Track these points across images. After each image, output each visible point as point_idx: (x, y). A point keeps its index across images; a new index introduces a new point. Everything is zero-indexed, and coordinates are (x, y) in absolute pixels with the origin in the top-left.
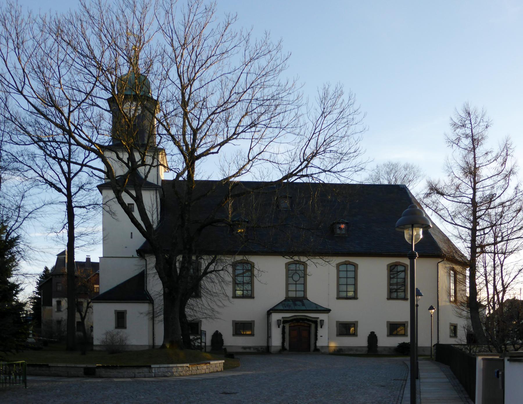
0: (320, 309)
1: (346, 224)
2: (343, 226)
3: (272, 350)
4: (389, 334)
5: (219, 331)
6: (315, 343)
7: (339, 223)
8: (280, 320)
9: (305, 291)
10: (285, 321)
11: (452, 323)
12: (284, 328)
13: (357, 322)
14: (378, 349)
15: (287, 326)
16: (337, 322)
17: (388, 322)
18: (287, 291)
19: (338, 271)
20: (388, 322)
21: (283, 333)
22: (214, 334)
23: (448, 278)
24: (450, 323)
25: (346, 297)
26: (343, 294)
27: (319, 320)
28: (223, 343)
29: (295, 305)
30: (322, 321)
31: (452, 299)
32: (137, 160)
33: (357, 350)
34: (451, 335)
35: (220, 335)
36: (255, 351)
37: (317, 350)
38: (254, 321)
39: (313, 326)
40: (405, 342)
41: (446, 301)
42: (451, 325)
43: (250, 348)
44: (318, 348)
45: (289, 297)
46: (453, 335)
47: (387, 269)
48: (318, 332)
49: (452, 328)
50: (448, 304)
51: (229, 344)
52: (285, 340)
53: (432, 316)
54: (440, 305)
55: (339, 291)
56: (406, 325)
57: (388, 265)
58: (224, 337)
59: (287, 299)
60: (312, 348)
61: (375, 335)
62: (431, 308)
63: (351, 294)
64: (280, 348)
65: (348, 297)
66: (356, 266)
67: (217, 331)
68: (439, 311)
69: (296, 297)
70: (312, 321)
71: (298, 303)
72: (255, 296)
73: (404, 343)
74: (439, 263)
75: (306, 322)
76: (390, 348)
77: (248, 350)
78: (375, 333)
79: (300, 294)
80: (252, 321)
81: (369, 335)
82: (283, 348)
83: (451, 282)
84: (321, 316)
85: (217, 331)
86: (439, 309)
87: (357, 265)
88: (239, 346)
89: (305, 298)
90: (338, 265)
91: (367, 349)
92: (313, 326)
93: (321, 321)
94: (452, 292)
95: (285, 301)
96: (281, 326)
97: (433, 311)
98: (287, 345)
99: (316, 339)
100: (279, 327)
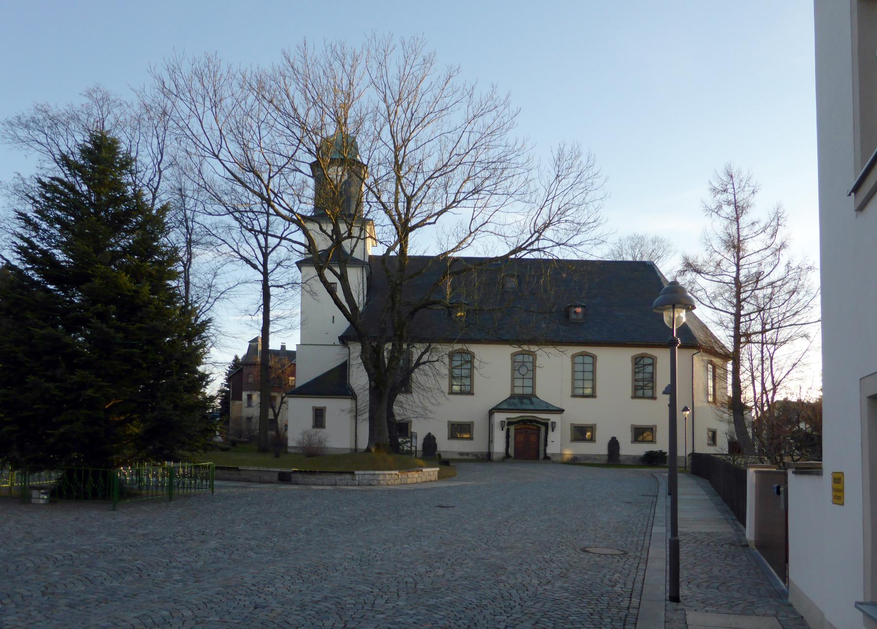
1: (582, 307)
2: (579, 310)
3: (494, 457)
6: (545, 450)
8: (505, 422)
9: (533, 387)
10: (510, 423)
14: (620, 458)
17: (632, 426)
18: (513, 387)
20: (632, 426)
21: (508, 437)
26: (580, 392)
27: (550, 423)
30: (554, 424)
31: (711, 399)
33: (595, 459)
35: (434, 438)
36: (474, 458)
37: (547, 458)
40: (654, 450)
42: (709, 430)
43: (467, 454)
44: (548, 455)
46: (712, 443)
47: (632, 362)
50: (706, 404)
55: (574, 388)
56: (654, 429)
57: (632, 357)
60: (542, 455)
61: (617, 441)
63: (588, 391)
66: (594, 357)
67: (430, 434)
71: (526, 401)
74: (694, 354)
76: (634, 457)
77: (465, 457)
78: (617, 439)
82: (507, 455)
84: (553, 418)
85: (430, 434)
86: (695, 410)
91: (607, 458)
92: (543, 429)
96: (505, 428)
98: (511, 451)
99: (546, 445)
100: (502, 430)
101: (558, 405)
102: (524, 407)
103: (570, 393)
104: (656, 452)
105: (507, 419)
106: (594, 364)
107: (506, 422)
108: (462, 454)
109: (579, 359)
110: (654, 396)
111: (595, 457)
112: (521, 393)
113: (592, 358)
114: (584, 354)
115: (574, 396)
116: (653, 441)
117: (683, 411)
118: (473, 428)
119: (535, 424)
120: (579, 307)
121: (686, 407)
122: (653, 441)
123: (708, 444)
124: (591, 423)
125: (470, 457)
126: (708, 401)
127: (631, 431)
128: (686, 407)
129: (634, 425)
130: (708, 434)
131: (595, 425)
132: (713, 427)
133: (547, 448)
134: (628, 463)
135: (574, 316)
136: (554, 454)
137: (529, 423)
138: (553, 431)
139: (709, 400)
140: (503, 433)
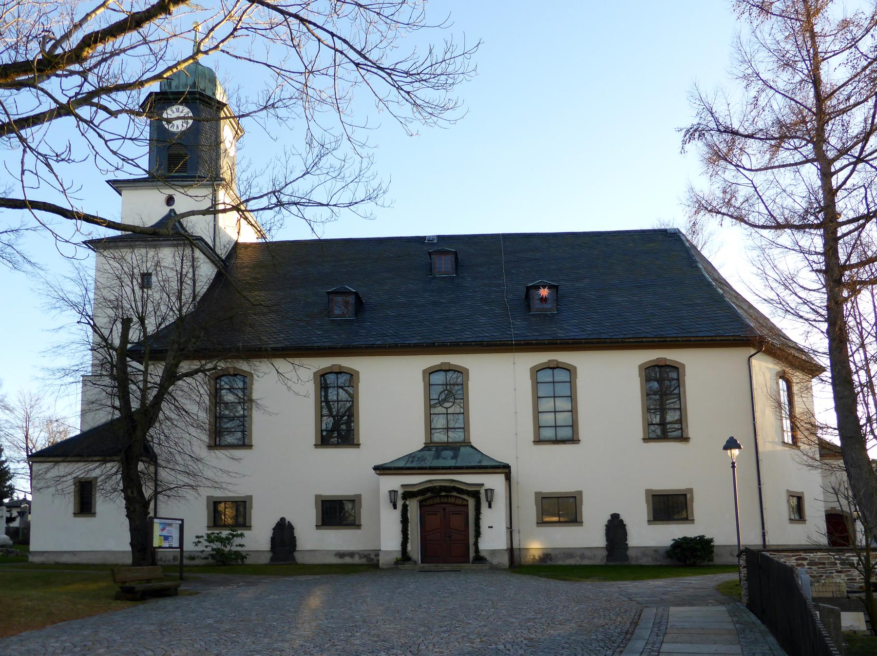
0: (484, 463)
1: (550, 287)
2: (544, 292)
3: (383, 560)
4: (320, 524)
5: (288, 519)
6: (476, 544)
7: (537, 287)
8: (395, 492)
9: (466, 429)
10: (408, 495)
11: (791, 490)
12: (405, 509)
13: (580, 493)
14: (630, 553)
15: (414, 506)
16: (537, 494)
17: (648, 492)
18: (430, 429)
19: (536, 383)
20: (648, 492)
21: (405, 521)
22: (827, 518)
23: (779, 422)
24: (788, 491)
25: (554, 438)
26: (548, 433)
27: (482, 492)
28: (295, 545)
29: (437, 456)
30: (490, 492)
31: (788, 439)
32: (261, 241)
33: (582, 556)
34: (793, 517)
35: (291, 528)
36: (364, 561)
37: (479, 559)
38: (359, 496)
39: (471, 503)
40: (689, 536)
41: (773, 442)
42: (791, 495)
43: (351, 554)
44: (482, 554)
45: (431, 443)
46: (797, 517)
47: (640, 375)
48: (482, 516)
49: (794, 501)
50: (780, 448)
51: (308, 547)
52: (408, 538)
53: (733, 467)
54: (760, 449)
55: (538, 427)
56: (688, 496)
57: (640, 367)
58: (298, 533)
59: (427, 447)
60: (472, 554)
61: (622, 521)
62: (732, 444)
63: (565, 433)
64: (399, 556)
65: (558, 438)
66: (571, 370)
67: (283, 520)
68: (760, 463)
69: (448, 442)
70: (468, 493)
71: (449, 453)
72: (361, 442)
73: (685, 538)
74: (751, 356)
75: (455, 494)
76: (656, 550)
77: (348, 560)
78: (622, 517)
79: (456, 436)
80: (356, 496)
81: (609, 521)
82: (405, 556)
83: (787, 407)
84: (495, 482)
85: (283, 520)
86: (760, 458)
87: (575, 368)
88: (328, 552)
89: (467, 443)
90: (536, 371)
91: (605, 553)
92: (471, 503)
93: (486, 490)
94: (784, 398)
95: (422, 450)
96: (400, 503)
97: (736, 452)
98: (414, 549)
99: (478, 534)
100: (395, 507)
101: (500, 456)
102: (441, 463)
103: (531, 438)
104: (691, 540)
105: (403, 486)
106: (572, 383)
107: (400, 492)
108: (341, 555)
109: (545, 376)
110: (684, 436)
111: (583, 552)
112: (446, 440)
113: (568, 373)
114: (554, 367)
115: (538, 441)
116: (687, 519)
117: (726, 448)
118: (251, 507)
119: (455, 494)
120: (544, 287)
121: (732, 438)
122: (687, 519)
123: (790, 519)
124: (244, 495)
125: (357, 560)
126: (784, 442)
127: (647, 502)
128: (732, 438)
129: (651, 490)
130: (788, 501)
131: (580, 493)
132: (797, 488)
133: (480, 540)
134: (644, 561)
135: (536, 305)
136: (493, 552)
137: (443, 494)
138: (490, 506)
139: (786, 441)
140: (397, 514)
